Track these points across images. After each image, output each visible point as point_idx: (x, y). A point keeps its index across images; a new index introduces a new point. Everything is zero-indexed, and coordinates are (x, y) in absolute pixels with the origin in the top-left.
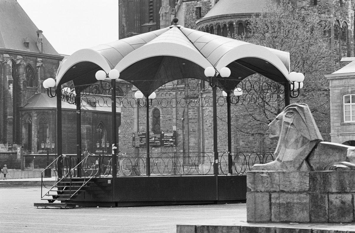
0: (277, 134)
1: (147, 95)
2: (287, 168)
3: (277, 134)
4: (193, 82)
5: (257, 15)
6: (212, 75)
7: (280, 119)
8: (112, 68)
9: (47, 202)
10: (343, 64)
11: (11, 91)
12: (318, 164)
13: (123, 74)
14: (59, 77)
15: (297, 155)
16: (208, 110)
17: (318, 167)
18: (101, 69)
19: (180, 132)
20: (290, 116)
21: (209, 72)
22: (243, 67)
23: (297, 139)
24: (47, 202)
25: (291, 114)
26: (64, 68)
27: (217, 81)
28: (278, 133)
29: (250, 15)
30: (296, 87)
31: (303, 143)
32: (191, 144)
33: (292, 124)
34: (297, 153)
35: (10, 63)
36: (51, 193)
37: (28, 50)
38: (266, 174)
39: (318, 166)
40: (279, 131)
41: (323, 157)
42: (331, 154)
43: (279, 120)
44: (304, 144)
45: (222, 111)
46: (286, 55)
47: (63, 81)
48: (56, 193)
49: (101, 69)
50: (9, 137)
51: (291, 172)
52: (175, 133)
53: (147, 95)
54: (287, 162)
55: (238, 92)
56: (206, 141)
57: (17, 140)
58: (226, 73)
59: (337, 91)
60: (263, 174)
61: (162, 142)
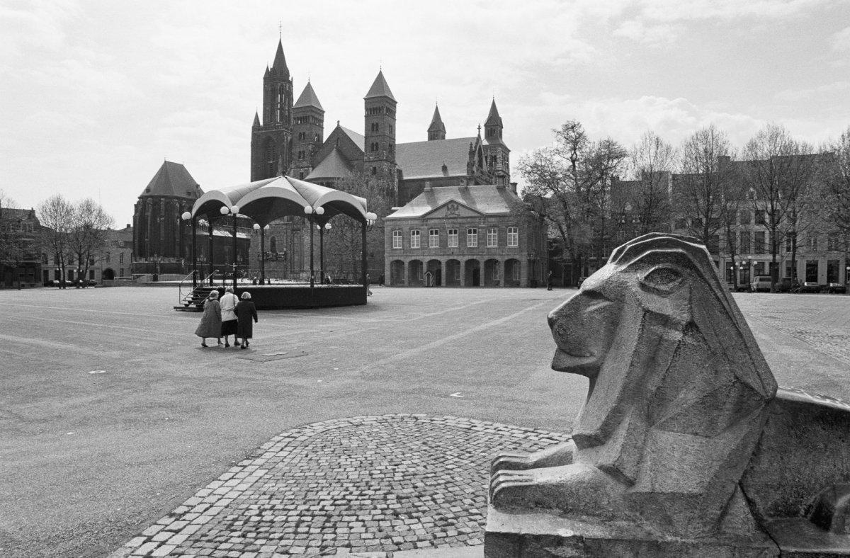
0: (592, 355)
1: (262, 226)
2: (668, 521)
3: (592, 355)
4: (297, 218)
5: (339, 178)
6: (311, 212)
7: (612, 296)
8: (234, 204)
9: (184, 306)
10: (394, 211)
11: (179, 222)
12: (778, 488)
13: (241, 211)
14: (194, 211)
15: (716, 466)
16: (307, 239)
17: (776, 506)
18: (224, 205)
19: (289, 252)
20: (663, 288)
21: (308, 209)
22: (333, 208)
23: (713, 394)
24: (184, 306)
25: (671, 281)
26: (198, 203)
27: (314, 217)
28: (596, 350)
29: (333, 178)
30: (371, 224)
31: (740, 411)
32: (295, 260)
33: (691, 326)
34: (714, 456)
35: (178, 205)
36: (187, 299)
37: (190, 197)
38: (576, 547)
39: (777, 497)
40: (601, 343)
41: (795, 459)
42: (822, 446)
43: (607, 299)
44: (743, 417)
45: (317, 239)
46: (364, 200)
47: (197, 214)
48: (191, 299)
49: (224, 205)
50: (177, 253)
51: (693, 545)
52: (285, 252)
53: (262, 226)
54: (674, 497)
55: (328, 226)
56: (305, 258)
57: (182, 255)
58: (320, 210)
59: (389, 228)
60: (559, 549)
61: (277, 258)
